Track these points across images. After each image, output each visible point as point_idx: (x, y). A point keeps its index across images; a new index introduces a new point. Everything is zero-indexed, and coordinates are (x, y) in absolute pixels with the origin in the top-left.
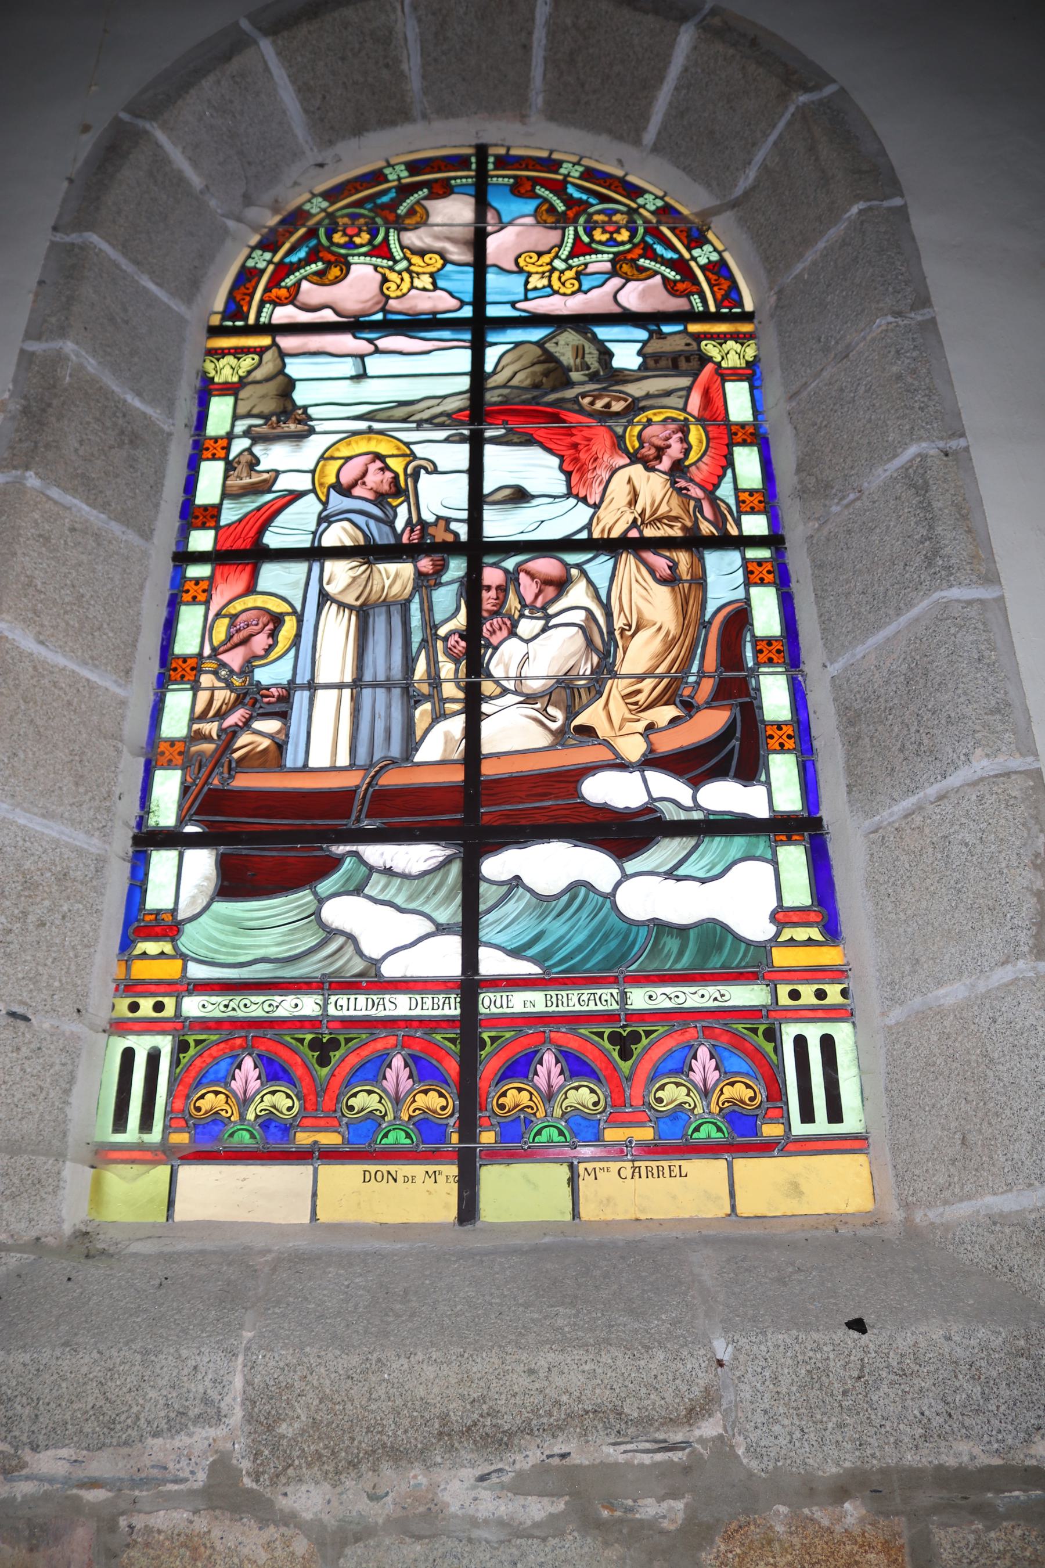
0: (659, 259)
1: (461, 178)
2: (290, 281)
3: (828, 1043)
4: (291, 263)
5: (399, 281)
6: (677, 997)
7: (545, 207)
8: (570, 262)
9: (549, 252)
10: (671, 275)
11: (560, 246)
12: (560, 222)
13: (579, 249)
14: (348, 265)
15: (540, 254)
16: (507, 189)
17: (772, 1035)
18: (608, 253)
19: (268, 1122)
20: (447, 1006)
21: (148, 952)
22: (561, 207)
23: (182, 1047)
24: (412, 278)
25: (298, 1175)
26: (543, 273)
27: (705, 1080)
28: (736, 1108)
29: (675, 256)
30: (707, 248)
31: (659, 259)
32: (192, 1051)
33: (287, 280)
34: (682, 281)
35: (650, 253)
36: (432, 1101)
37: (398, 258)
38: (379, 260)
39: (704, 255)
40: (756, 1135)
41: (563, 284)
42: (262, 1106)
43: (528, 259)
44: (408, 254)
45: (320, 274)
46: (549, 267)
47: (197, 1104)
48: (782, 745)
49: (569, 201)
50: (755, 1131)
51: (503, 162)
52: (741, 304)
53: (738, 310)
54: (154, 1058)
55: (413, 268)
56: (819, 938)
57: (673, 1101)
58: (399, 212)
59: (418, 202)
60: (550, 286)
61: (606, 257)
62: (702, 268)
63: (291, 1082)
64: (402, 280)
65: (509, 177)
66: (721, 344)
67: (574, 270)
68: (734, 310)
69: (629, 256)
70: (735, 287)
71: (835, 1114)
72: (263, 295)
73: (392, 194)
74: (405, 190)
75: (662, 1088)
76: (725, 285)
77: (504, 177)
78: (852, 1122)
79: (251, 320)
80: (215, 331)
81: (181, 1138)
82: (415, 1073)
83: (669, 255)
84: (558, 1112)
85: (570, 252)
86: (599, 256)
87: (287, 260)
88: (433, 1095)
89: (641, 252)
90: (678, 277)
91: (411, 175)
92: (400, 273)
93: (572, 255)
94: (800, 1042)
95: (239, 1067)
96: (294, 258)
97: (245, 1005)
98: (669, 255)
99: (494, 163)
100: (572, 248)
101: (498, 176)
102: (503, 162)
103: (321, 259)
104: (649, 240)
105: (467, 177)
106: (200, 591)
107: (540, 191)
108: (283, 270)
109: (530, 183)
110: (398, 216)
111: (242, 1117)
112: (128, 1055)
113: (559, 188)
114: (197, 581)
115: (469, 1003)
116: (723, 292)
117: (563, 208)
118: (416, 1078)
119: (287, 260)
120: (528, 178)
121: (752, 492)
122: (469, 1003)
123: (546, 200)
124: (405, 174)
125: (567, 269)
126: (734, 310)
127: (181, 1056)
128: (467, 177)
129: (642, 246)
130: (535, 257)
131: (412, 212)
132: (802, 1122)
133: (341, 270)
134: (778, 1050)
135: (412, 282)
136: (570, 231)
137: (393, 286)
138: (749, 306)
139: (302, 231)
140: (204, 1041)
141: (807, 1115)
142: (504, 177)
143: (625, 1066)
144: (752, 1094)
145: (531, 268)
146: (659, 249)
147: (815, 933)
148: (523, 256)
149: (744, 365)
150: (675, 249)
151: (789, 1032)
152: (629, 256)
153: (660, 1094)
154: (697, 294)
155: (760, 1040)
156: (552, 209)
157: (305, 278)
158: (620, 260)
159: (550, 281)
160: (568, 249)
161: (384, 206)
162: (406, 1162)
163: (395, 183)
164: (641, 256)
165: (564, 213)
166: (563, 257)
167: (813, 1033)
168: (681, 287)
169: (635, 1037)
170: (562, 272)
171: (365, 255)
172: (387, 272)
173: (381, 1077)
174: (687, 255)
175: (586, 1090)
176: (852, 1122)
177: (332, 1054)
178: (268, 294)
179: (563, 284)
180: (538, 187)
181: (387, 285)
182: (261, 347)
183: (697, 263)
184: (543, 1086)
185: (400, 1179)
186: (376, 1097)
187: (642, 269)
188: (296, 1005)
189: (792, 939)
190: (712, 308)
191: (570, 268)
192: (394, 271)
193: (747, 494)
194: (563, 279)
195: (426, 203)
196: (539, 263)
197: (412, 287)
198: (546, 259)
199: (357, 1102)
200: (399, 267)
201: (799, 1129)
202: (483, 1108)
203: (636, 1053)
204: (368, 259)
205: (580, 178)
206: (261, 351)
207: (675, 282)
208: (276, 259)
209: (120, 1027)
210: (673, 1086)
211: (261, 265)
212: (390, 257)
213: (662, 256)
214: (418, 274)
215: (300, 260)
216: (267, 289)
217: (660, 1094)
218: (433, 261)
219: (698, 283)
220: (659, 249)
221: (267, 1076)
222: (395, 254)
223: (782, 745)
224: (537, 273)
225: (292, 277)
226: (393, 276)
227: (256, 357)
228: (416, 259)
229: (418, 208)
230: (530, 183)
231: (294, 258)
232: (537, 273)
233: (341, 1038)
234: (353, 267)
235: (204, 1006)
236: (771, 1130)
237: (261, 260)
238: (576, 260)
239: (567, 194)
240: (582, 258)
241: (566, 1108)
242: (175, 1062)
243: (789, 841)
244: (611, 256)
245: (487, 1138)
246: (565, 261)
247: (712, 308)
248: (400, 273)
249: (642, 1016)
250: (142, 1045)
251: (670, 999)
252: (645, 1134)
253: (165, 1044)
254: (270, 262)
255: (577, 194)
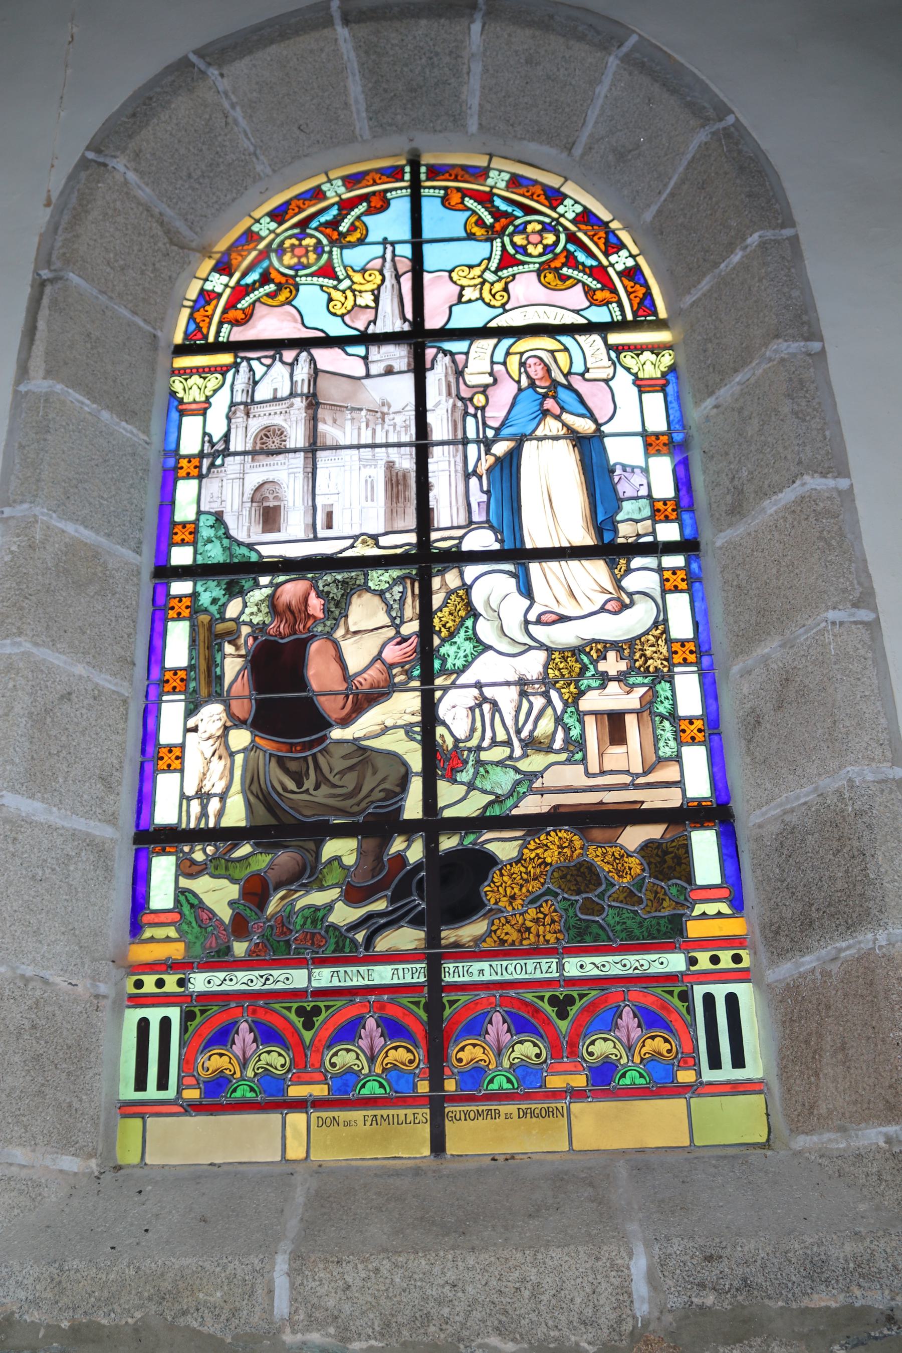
0: (581, 267)
1: (396, 189)
2: (244, 304)
3: (732, 1000)
4: (247, 285)
5: (343, 300)
6: (604, 966)
7: (473, 219)
8: (500, 273)
9: (479, 265)
10: (595, 285)
11: (489, 259)
12: (492, 234)
13: (507, 261)
14: (297, 287)
15: (470, 267)
16: (439, 200)
17: (685, 996)
18: (535, 263)
19: (266, 1075)
20: (456, 974)
21: (156, 937)
22: (489, 220)
23: (188, 1017)
24: (355, 296)
25: (677, 1105)
26: (475, 286)
27: (498, 1041)
28: (524, 1063)
29: (595, 263)
30: (624, 253)
31: (581, 267)
32: (198, 1019)
33: (243, 302)
34: (602, 290)
35: (572, 262)
36: (401, 1055)
37: (341, 277)
38: (326, 280)
39: (621, 261)
40: (283, 1096)
41: (494, 296)
42: (258, 1065)
43: (461, 273)
44: (351, 273)
45: (272, 295)
46: (480, 280)
47: (333, 1061)
48: (693, 738)
49: (497, 214)
50: (283, 1091)
51: (435, 172)
52: (655, 313)
53: (653, 318)
54: (165, 1023)
55: (355, 287)
56: (729, 912)
57: (472, 1060)
58: (341, 228)
59: (358, 218)
60: (481, 298)
61: (532, 267)
62: (620, 274)
63: (535, 1032)
64: (346, 298)
65: (440, 188)
66: (638, 355)
67: (503, 281)
68: (648, 318)
69: (553, 265)
70: (648, 294)
71: (738, 1061)
72: (221, 317)
73: (334, 211)
74: (346, 206)
75: (592, 1043)
76: (641, 291)
77: (434, 188)
78: (754, 1069)
79: (211, 339)
80: (181, 350)
81: (192, 1094)
82: (386, 1032)
83: (590, 262)
84: (506, 1064)
85: (499, 264)
86: (526, 266)
87: (243, 282)
88: (528, 1045)
89: (563, 260)
90: (599, 286)
91: (349, 190)
92: (344, 292)
93: (500, 268)
94: (709, 999)
95: (620, 1017)
96: (249, 280)
97: (252, 981)
98: (590, 262)
99: (403, 173)
100: (500, 260)
101: (430, 188)
102: (435, 172)
103: (272, 281)
104: (571, 247)
105: (401, 188)
106: (183, 607)
107: (469, 202)
108: (241, 291)
109: (459, 195)
110: (341, 234)
111: (499, 1064)
112: (143, 1025)
113: (485, 199)
114: (180, 598)
115: (434, 972)
116: (638, 300)
117: (492, 220)
118: (513, 1032)
119: (243, 282)
120: (458, 189)
121: (665, 502)
122: (434, 972)
123: (474, 212)
124: (342, 190)
125: (497, 281)
126: (648, 318)
127: (189, 1023)
128: (401, 188)
129: (565, 254)
130: (466, 269)
131: (353, 228)
132: (711, 1068)
133: (291, 292)
134: (691, 1010)
135: (355, 301)
136: (497, 243)
137: (339, 305)
138: (663, 314)
139: (254, 254)
140: (586, 995)
141: (715, 1063)
142: (434, 188)
143: (307, 1036)
144: (412, 1058)
145: (464, 282)
146: (581, 257)
147: (725, 908)
148: (456, 270)
149: (659, 375)
150: (591, 254)
151: (699, 991)
152: (553, 265)
153: (460, 1055)
154: (616, 302)
155: (676, 1001)
156: (480, 222)
157: (584, 284)
158: (544, 270)
159: (481, 294)
160: (497, 261)
161: (327, 224)
162: (349, 1108)
163: (337, 199)
164: (564, 265)
165: (492, 226)
166: (493, 269)
167: (720, 991)
168: (599, 295)
169: (317, 1011)
170: (492, 284)
171: (312, 275)
172: (332, 291)
173: (483, 1032)
174: (605, 262)
175: (275, 1055)
176: (754, 1069)
177: (315, 1019)
178: (225, 316)
179: (494, 296)
180: (467, 199)
181: (332, 304)
182: (225, 366)
183: (615, 269)
184: (240, 1054)
185: (341, 1124)
186: (353, 1055)
187: (564, 278)
188: (209, 982)
189: (704, 914)
190: (630, 317)
191: (501, 278)
192: (338, 290)
193: (661, 503)
194: (493, 292)
195: (364, 218)
196: (471, 276)
197: (355, 305)
198: (477, 271)
199: (465, 1056)
200: (342, 286)
201: (709, 1075)
202: (447, 1061)
203: (317, 1025)
204: (315, 279)
205: (508, 188)
206: (223, 370)
207: (595, 291)
208: (232, 283)
209: (138, 1001)
210: (470, 1047)
211: (219, 289)
212: (334, 276)
213: (583, 264)
214: (360, 292)
215: (255, 282)
216: (225, 311)
217: (460, 1055)
218: (373, 276)
219: (614, 291)
220: (581, 257)
221: (646, 1024)
222: (339, 273)
223: (177, 758)
224: (469, 286)
225: (247, 298)
226: (336, 295)
227: (219, 376)
228: (357, 277)
229: (357, 224)
230: (459, 195)
231: (249, 280)
232: (469, 286)
233: (196, 1010)
234: (301, 287)
235: (288, 979)
236: (685, 1076)
237: (218, 282)
238: (505, 271)
239: (494, 206)
240: (510, 269)
241: (387, 1065)
242: (184, 1029)
243: (703, 827)
244: (537, 266)
245: (450, 1086)
246: (495, 272)
247: (630, 317)
248: (344, 292)
249: (572, 982)
250: (154, 1015)
251: (598, 967)
252: (320, 1091)
253: (174, 1013)
254: (226, 286)
255: (503, 206)
